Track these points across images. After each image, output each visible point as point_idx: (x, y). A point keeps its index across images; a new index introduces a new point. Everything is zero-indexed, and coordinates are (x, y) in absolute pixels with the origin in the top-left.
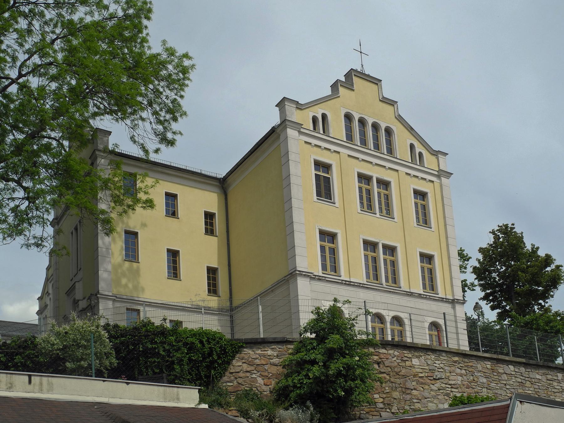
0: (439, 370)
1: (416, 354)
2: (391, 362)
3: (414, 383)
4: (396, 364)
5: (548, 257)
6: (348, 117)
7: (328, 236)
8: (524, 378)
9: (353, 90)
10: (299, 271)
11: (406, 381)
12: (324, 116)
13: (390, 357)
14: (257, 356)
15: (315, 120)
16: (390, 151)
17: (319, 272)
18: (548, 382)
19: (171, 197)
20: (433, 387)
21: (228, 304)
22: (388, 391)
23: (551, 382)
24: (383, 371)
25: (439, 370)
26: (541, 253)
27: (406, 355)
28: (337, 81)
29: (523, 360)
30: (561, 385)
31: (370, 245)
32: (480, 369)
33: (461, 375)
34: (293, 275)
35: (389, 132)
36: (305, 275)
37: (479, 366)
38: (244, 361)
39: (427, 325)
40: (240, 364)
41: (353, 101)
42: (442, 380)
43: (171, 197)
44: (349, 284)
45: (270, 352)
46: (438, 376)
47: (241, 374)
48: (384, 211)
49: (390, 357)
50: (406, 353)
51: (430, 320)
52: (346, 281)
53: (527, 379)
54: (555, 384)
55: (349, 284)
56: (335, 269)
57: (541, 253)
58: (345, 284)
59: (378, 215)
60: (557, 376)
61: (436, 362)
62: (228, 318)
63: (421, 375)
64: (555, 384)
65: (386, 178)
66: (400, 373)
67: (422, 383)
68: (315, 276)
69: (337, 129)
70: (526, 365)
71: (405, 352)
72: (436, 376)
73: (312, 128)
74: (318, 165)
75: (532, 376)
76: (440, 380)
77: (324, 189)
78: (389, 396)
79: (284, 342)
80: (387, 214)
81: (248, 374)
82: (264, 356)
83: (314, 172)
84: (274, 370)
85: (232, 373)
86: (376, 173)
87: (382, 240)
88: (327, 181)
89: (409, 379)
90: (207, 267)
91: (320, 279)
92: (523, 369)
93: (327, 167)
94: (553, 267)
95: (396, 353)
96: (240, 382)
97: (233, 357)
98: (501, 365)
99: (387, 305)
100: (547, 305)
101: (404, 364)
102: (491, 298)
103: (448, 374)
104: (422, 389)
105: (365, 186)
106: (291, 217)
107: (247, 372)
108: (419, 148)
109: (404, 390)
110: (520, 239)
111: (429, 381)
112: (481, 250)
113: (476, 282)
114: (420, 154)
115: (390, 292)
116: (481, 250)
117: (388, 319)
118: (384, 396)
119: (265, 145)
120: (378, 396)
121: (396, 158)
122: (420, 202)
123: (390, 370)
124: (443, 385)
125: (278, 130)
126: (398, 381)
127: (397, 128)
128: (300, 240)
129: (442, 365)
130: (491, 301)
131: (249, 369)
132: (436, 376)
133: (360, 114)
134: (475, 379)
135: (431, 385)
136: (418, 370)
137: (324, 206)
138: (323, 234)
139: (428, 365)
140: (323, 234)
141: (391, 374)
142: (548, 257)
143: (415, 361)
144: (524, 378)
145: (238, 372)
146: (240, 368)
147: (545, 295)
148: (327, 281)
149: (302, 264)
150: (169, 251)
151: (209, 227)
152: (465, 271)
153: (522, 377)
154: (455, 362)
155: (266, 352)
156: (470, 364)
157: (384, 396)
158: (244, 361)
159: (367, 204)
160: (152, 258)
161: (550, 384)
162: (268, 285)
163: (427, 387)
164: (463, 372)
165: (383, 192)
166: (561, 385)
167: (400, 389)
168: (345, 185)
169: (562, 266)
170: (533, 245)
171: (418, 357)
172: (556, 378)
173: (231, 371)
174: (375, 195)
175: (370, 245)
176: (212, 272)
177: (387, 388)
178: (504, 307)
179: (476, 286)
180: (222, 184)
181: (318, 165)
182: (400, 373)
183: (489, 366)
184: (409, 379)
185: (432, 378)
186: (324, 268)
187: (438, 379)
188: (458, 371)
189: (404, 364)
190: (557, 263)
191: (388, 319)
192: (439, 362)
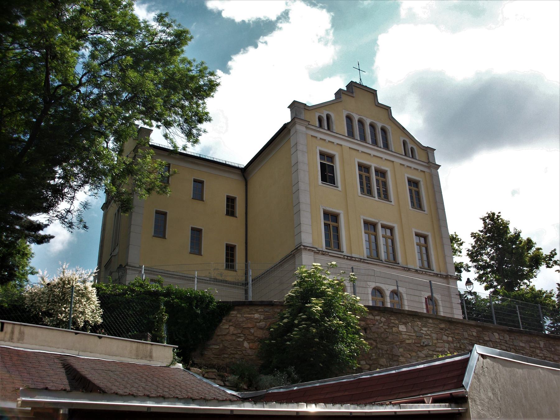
0: (427, 337)
1: (404, 320)
2: (378, 328)
3: (401, 350)
4: (383, 330)
5: (529, 241)
6: (349, 118)
7: (331, 218)
8: (508, 346)
9: (353, 97)
10: (304, 246)
11: (393, 347)
12: (328, 117)
13: (377, 323)
14: (244, 319)
15: (320, 119)
16: (386, 146)
17: (324, 248)
18: (532, 349)
19: (199, 183)
20: (421, 354)
21: (244, 278)
22: (375, 357)
23: (534, 350)
24: (369, 336)
25: (427, 337)
26: (524, 237)
27: (393, 321)
28: (340, 90)
29: (508, 328)
30: (543, 352)
31: (370, 226)
32: (467, 336)
33: (448, 342)
34: (298, 250)
35: (384, 130)
36: (309, 250)
37: (465, 333)
38: (231, 324)
39: (370, 291)
40: (227, 327)
41: (358, 109)
42: (430, 348)
43: (199, 183)
44: (350, 258)
45: (257, 316)
46: (426, 343)
47: (228, 338)
48: (382, 196)
49: (377, 323)
50: (393, 319)
51: (373, 285)
52: (348, 256)
53: (511, 347)
54: (538, 351)
55: (350, 258)
56: (338, 247)
57: (524, 237)
58: (347, 259)
59: (377, 198)
60: (539, 344)
61: (423, 329)
62: (243, 292)
63: (408, 342)
64: (538, 351)
65: (384, 168)
66: (387, 340)
67: (409, 350)
68: (319, 251)
69: (340, 126)
70: (510, 332)
71: (392, 318)
72: (423, 343)
73: (317, 124)
74: (323, 155)
75: (516, 344)
76: (428, 347)
77: (328, 175)
78: (375, 362)
79: (270, 304)
80: (385, 198)
81: (234, 338)
82: (251, 319)
83: (319, 161)
84: (260, 334)
85: (219, 336)
86: (373, 164)
87: (381, 221)
88: (332, 169)
89: (396, 345)
90: (226, 244)
91: (324, 254)
92: (507, 337)
93: (331, 158)
94: (534, 249)
95: (383, 319)
96: (226, 345)
97: (220, 321)
98: (487, 333)
99: (387, 280)
100: (531, 285)
101: (391, 331)
102: (484, 279)
103: (435, 341)
104: (409, 356)
105: (364, 174)
106: (298, 198)
107: (233, 334)
108: (410, 146)
109: (391, 357)
110: (505, 226)
111: (415, 348)
112: (473, 235)
113: (470, 264)
114: (412, 149)
115: (389, 267)
116: (473, 235)
117: (388, 293)
118: (371, 362)
119: (278, 139)
120: (365, 363)
121: (392, 151)
122: (414, 189)
123: (376, 336)
124: (431, 353)
125: (289, 126)
126: (385, 347)
127: (390, 128)
128: (306, 218)
129: (429, 332)
130: (484, 281)
131: (235, 332)
132: (423, 343)
133: (359, 115)
134: (462, 346)
135: (419, 352)
136: (405, 336)
137: (327, 188)
138: (327, 214)
139: (415, 331)
140: (327, 214)
141: (378, 340)
142: (529, 241)
143: (402, 328)
144: (508, 346)
145: (225, 335)
146: (227, 331)
147: (529, 276)
148: (330, 256)
149: (307, 239)
150: (193, 229)
151: (230, 209)
152: (461, 254)
153: (506, 345)
154: (442, 329)
155: (253, 316)
156: (456, 331)
157: (371, 362)
158: (231, 324)
159: (367, 190)
160: (178, 235)
161: (533, 352)
162: (278, 260)
163: (414, 354)
164: (450, 339)
165: (381, 179)
166: (543, 352)
167: (387, 355)
168: (346, 172)
169: (541, 249)
170: (515, 229)
171: (405, 324)
172: (538, 346)
173: (218, 334)
174: (372, 182)
175: (370, 226)
176: (230, 250)
177: (374, 355)
178: (495, 287)
179: (470, 267)
180: (244, 172)
181: (323, 155)
182: (387, 340)
183: (474, 334)
184: (396, 345)
185: (419, 345)
186: (328, 244)
187: (426, 346)
188: (445, 338)
189: (391, 331)
190: (537, 246)
191: (388, 293)
192: (426, 329)
